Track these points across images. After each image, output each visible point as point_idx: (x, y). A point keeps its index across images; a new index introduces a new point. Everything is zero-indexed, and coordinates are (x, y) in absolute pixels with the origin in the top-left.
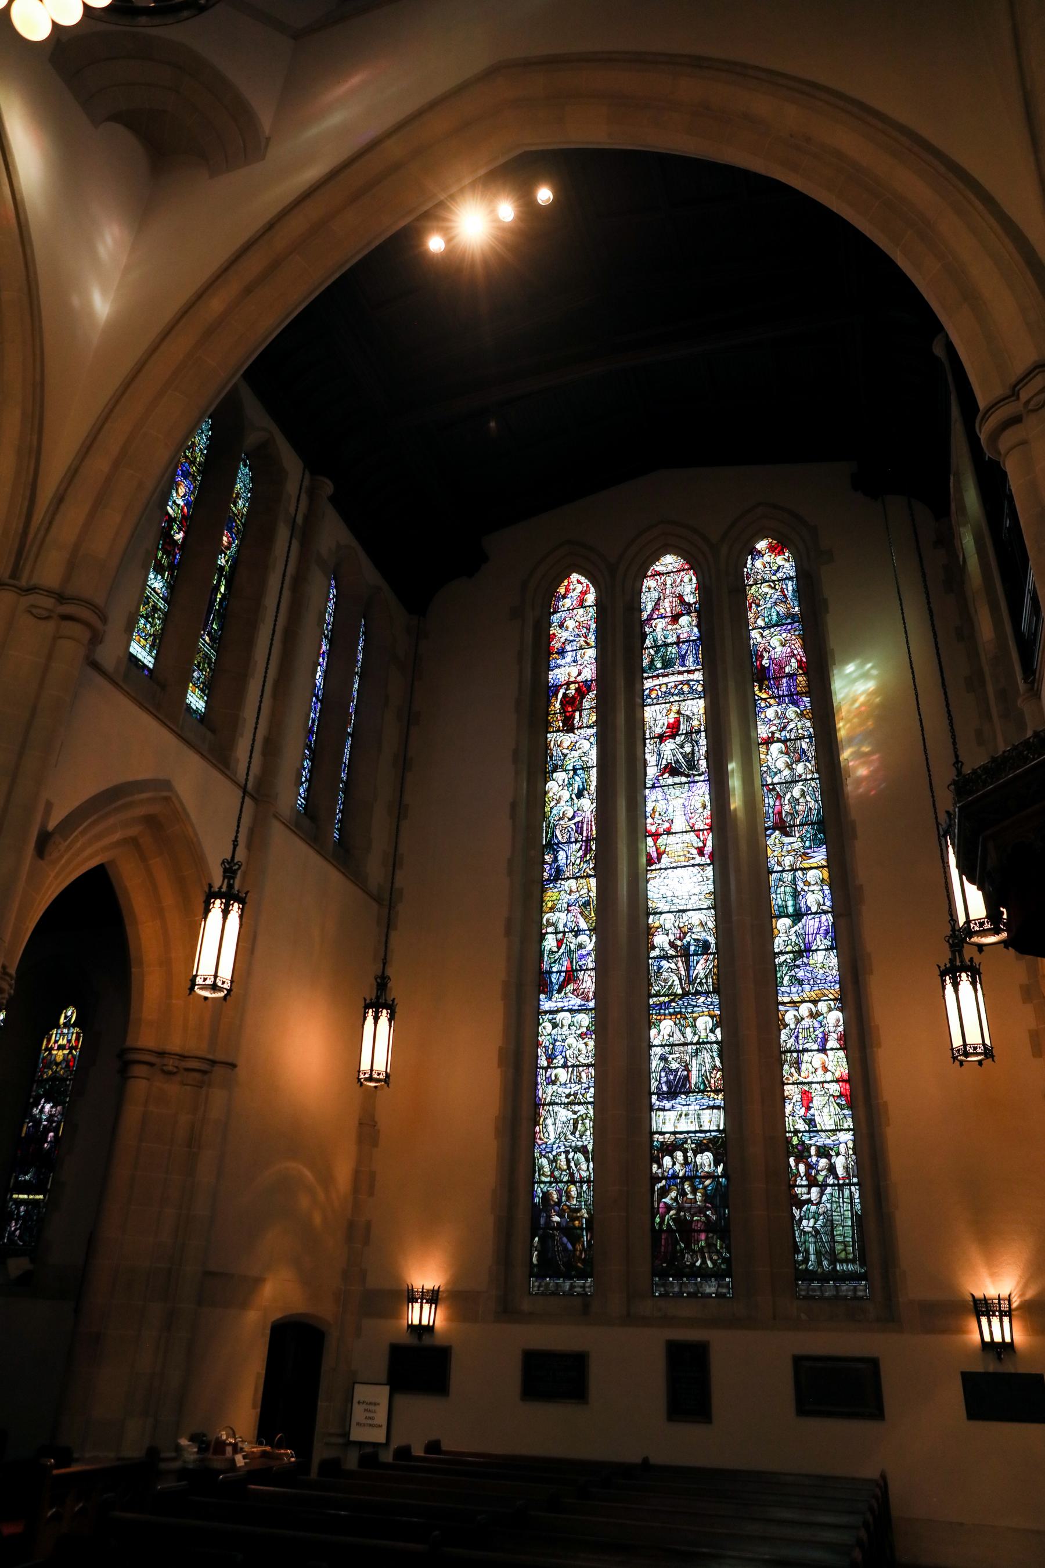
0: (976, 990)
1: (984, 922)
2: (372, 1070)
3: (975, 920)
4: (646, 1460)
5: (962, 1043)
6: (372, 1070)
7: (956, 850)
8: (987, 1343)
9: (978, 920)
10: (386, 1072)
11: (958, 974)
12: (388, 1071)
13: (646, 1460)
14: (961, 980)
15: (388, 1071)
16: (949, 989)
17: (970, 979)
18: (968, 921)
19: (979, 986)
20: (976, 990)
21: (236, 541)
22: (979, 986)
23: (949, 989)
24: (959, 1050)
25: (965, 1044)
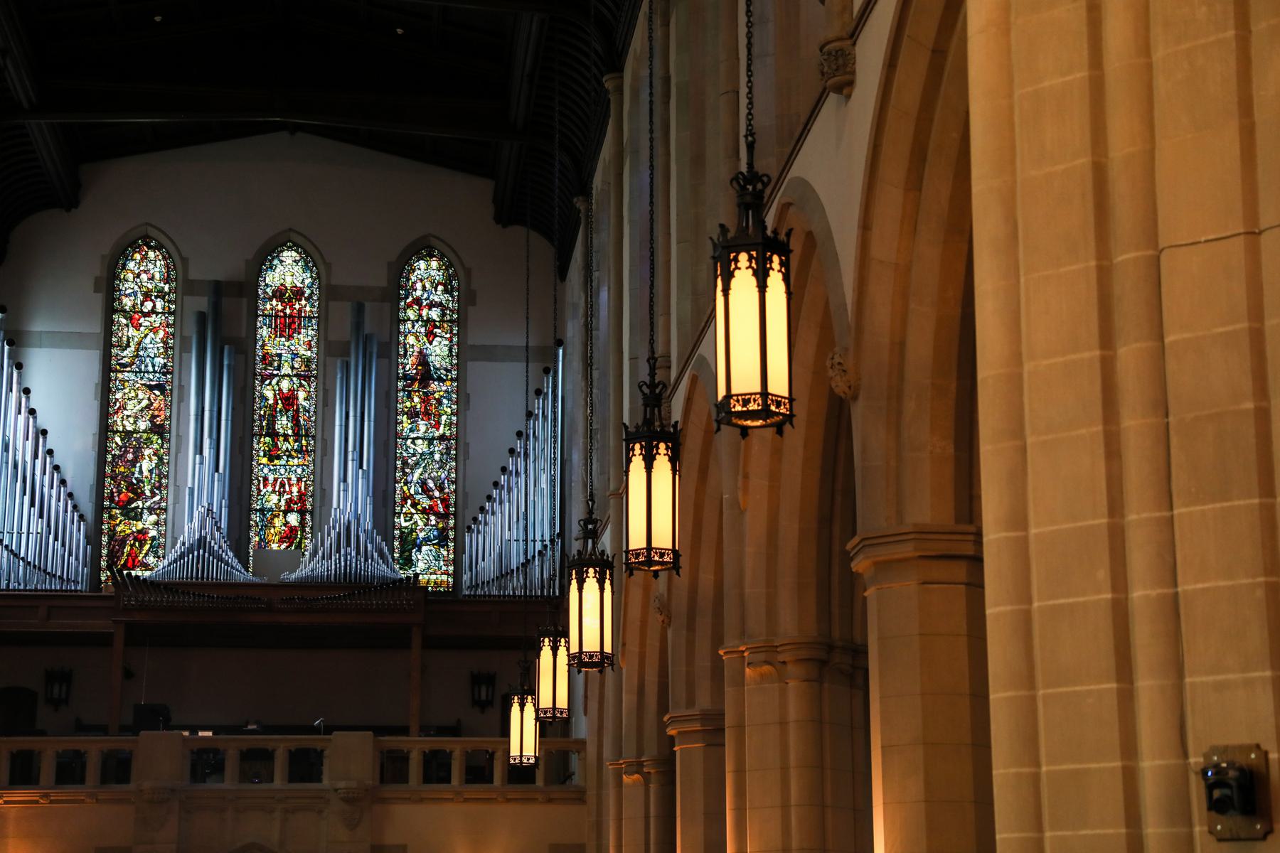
0: (602, 589)
1: (749, 399)
2: (521, 756)
3: (737, 395)
4: (681, 567)
5: (645, 546)
6: (521, 756)
7: (959, 25)
8: (768, 238)
9: (741, 395)
10: (535, 756)
11: (585, 569)
12: (537, 755)
13: (681, 567)
14: (587, 577)
15: (537, 755)
16: (637, 465)
17: (597, 576)
18: (729, 396)
19: (608, 583)
20: (602, 589)
21: (299, 505)
22: (608, 583)
23: (637, 465)
24: (637, 556)
25: (649, 547)
